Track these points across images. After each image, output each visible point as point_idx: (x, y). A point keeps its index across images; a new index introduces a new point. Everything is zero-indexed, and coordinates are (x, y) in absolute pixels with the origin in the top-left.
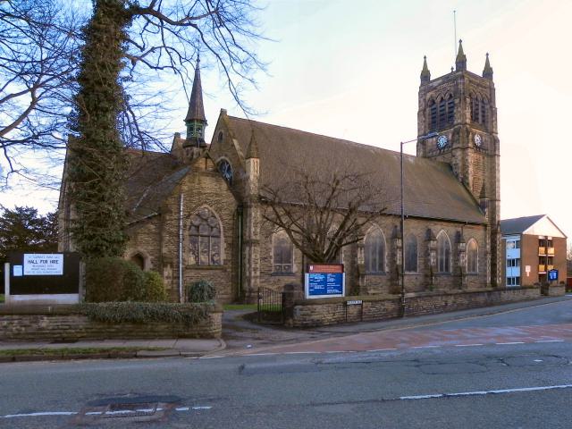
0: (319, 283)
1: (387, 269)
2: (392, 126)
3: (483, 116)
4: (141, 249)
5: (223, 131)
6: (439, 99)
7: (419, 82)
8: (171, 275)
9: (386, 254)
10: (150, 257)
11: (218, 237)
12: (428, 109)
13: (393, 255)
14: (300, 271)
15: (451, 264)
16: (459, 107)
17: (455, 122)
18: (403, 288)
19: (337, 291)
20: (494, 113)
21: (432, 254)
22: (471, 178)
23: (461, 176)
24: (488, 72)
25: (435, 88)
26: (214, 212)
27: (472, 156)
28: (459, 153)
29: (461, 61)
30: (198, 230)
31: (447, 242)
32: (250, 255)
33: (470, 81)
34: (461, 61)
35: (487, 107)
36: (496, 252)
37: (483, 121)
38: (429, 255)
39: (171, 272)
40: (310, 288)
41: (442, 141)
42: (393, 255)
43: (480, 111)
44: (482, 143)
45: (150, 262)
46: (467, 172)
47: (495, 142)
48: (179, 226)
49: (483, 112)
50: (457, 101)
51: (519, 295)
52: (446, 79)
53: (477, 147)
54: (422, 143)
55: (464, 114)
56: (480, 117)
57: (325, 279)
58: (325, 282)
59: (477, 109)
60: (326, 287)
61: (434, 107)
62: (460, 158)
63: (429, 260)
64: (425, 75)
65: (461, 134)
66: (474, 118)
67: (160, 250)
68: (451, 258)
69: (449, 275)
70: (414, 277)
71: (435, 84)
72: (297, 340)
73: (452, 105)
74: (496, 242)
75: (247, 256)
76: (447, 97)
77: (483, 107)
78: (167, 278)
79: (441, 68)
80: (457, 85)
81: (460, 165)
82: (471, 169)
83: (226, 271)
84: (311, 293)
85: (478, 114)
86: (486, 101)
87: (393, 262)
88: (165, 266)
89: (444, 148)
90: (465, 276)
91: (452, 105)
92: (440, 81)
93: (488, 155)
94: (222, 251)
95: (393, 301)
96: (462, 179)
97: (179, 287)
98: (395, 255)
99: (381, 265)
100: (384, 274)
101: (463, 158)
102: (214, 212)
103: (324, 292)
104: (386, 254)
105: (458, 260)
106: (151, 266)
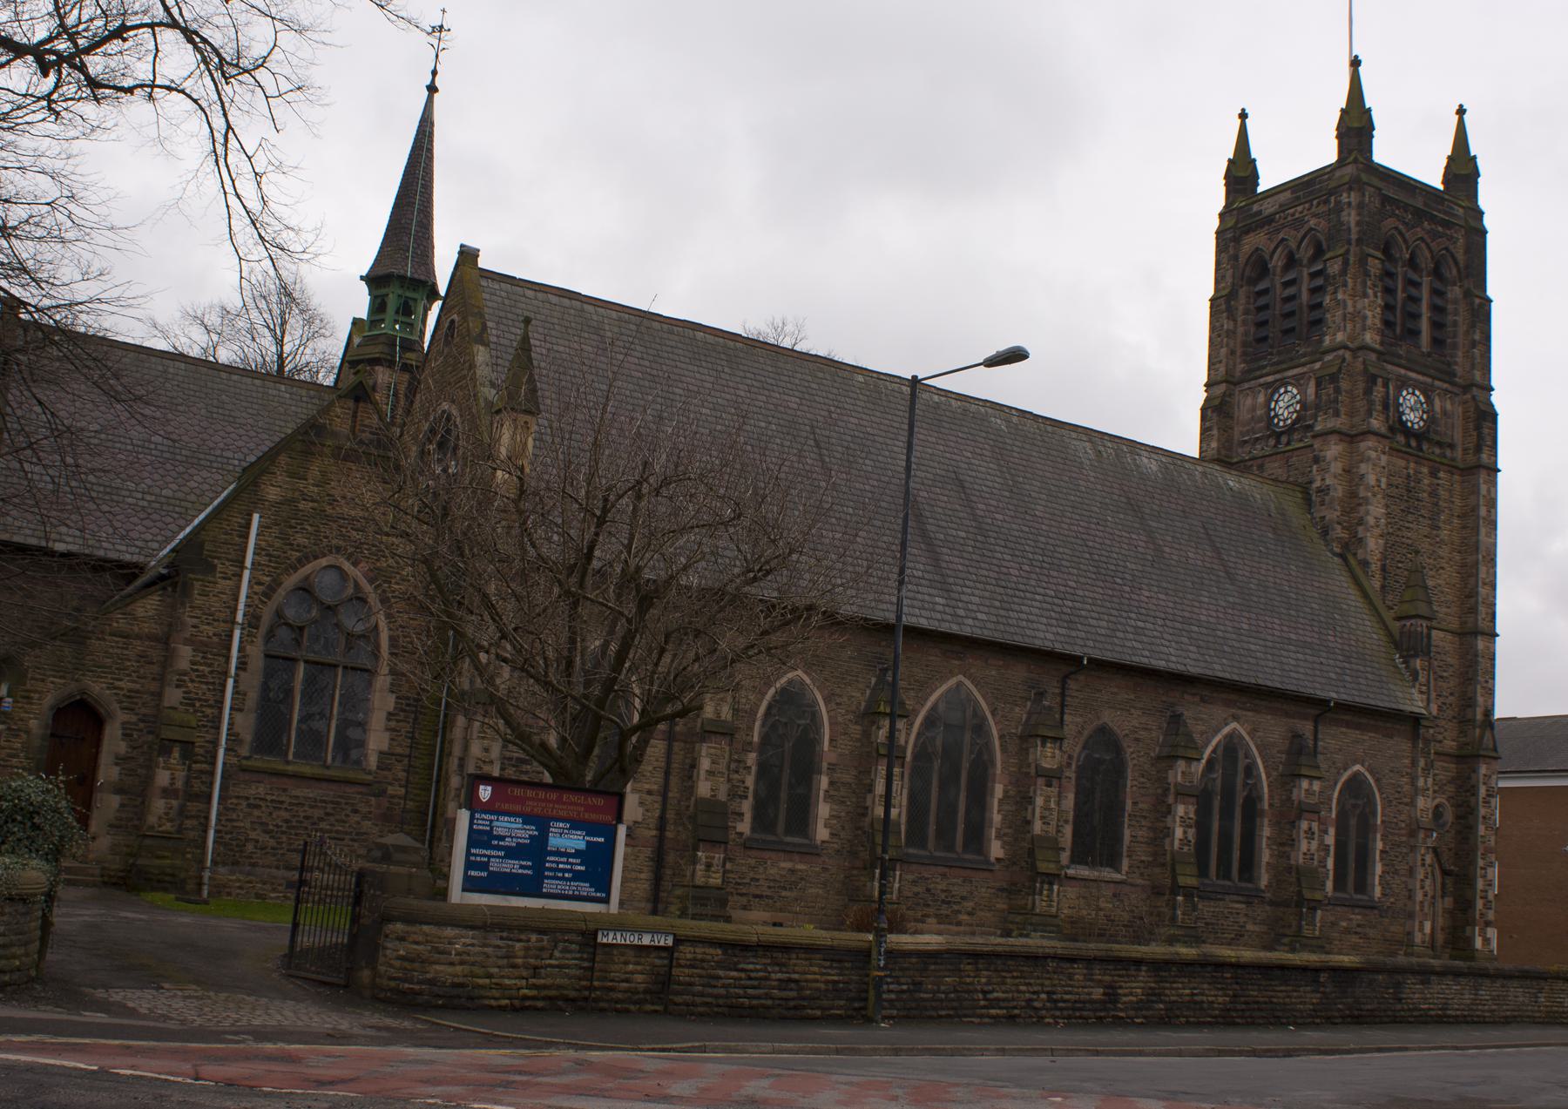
0: (511, 853)
1: (996, 850)
2: (1135, 355)
3: (1436, 325)
4: (97, 688)
5: (455, 317)
6: (1277, 262)
7: (1216, 198)
8: (179, 784)
9: (999, 791)
10: (122, 716)
11: (371, 673)
12: (1242, 292)
13: (1021, 800)
14: (653, 822)
15: (1265, 856)
16: (1350, 276)
17: (1327, 340)
18: (880, 911)
19: (585, 888)
20: (1480, 311)
21: (1180, 810)
22: (1373, 545)
23: (1338, 532)
24: (1462, 169)
25: (1270, 220)
26: (364, 583)
27: (1376, 465)
28: (1333, 451)
29: (1356, 126)
30: (298, 643)
31: (1250, 770)
32: (466, 748)
33: (1385, 199)
34: (1356, 126)
35: (1455, 292)
36: (1472, 828)
37: (1437, 342)
38: (1169, 811)
39: (181, 775)
40: (469, 865)
41: (1286, 405)
42: (1021, 800)
43: (1424, 308)
44: (1431, 421)
45: (117, 725)
46: (1361, 522)
47: (1484, 419)
48: (234, 622)
49: (1437, 309)
50: (1334, 268)
51: (1455, 994)
52: (1306, 187)
53: (1408, 432)
54: (1216, 412)
55: (1354, 317)
56: (1424, 325)
57: (540, 841)
58: (536, 850)
59: (1416, 300)
60: (539, 868)
61: (1261, 286)
62: (1336, 467)
63: (1168, 832)
64: (1241, 172)
65: (1344, 385)
66: (1399, 325)
67: (159, 695)
68: (1266, 831)
69: (1252, 897)
70: (1108, 891)
71: (1268, 208)
72: (334, 1037)
73: (1319, 282)
74: (1473, 790)
75: (457, 750)
76: (1305, 253)
77: (1435, 292)
78: (167, 793)
79: (1295, 150)
80: (1339, 209)
81: (1339, 492)
82: (1376, 511)
83: (383, 793)
84: (470, 885)
85: (1416, 316)
86: (1451, 272)
87: (1019, 824)
88: (165, 751)
89: (1290, 430)
90: (1314, 906)
91: (1319, 282)
92: (1288, 194)
93: (1452, 468)
94: (378, 721)
95: (834, 955)
96: (1346, 546)
97: (205, 829)
98: (1030, 800)
99: (976, 837)
100: (986, 867)
101: (1347, 471)
102: (364, 583)
103: (531, 887)
104: (999, 791)
105: (1292, 842)
106: (122, 747)
